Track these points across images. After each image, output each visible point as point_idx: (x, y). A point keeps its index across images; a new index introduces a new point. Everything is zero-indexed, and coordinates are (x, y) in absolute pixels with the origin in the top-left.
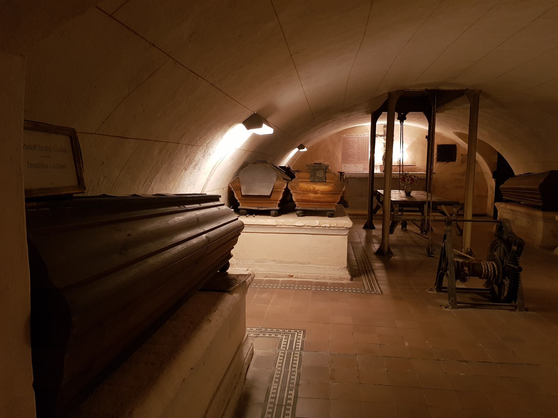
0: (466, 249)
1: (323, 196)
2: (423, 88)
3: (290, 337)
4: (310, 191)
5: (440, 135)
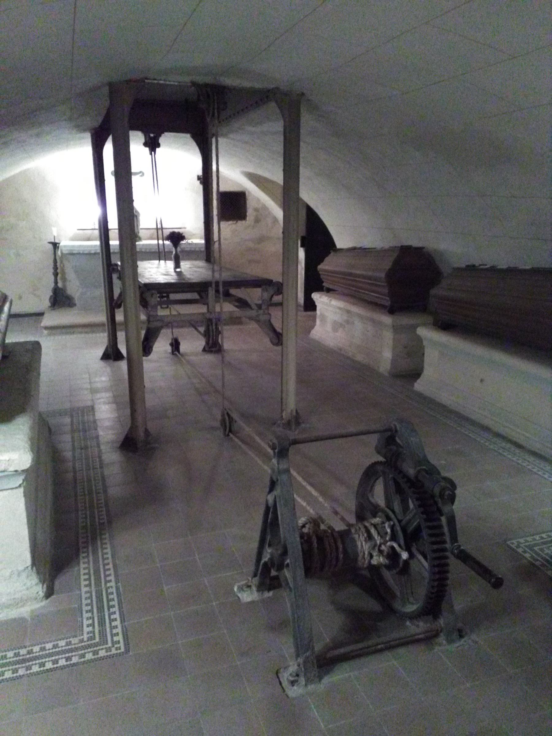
0: (289, 411)
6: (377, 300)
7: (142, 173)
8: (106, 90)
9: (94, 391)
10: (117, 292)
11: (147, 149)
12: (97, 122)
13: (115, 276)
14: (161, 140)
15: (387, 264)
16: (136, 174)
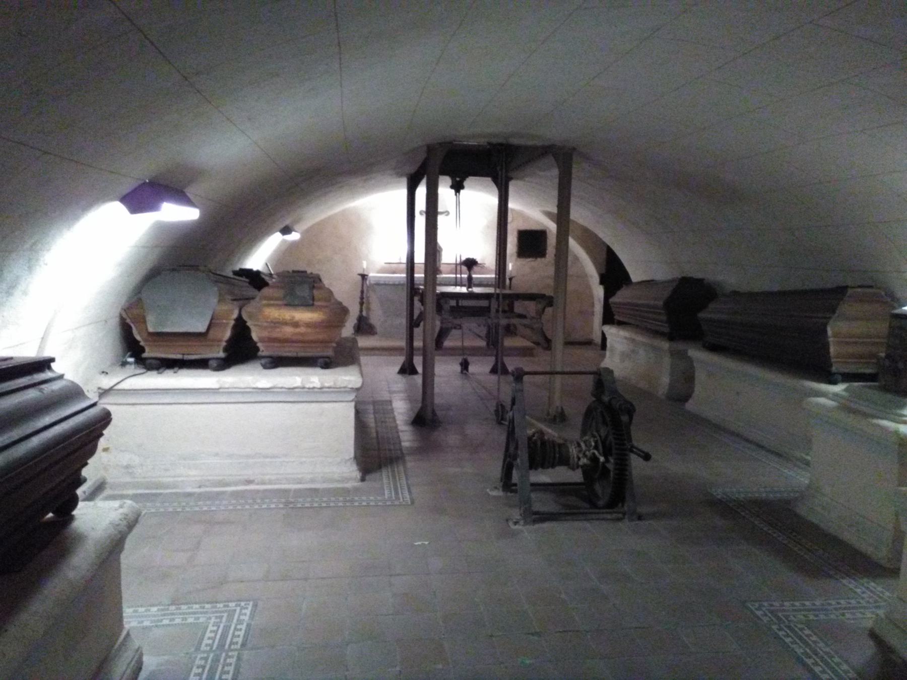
1: (309, 330)
2: (483, 141)
3: (224, 620)
4: (285, 323)
5: (520, 214)
6: (658, 328)
7: (447, 213)
8: (425, 149)
9: (391, 392)
10: (416, 313)
11: (453, 191)
12: (412, 169)
13: (416, 299)
14: (465, 183)
15: (666, 294)
16: (442, 213)
